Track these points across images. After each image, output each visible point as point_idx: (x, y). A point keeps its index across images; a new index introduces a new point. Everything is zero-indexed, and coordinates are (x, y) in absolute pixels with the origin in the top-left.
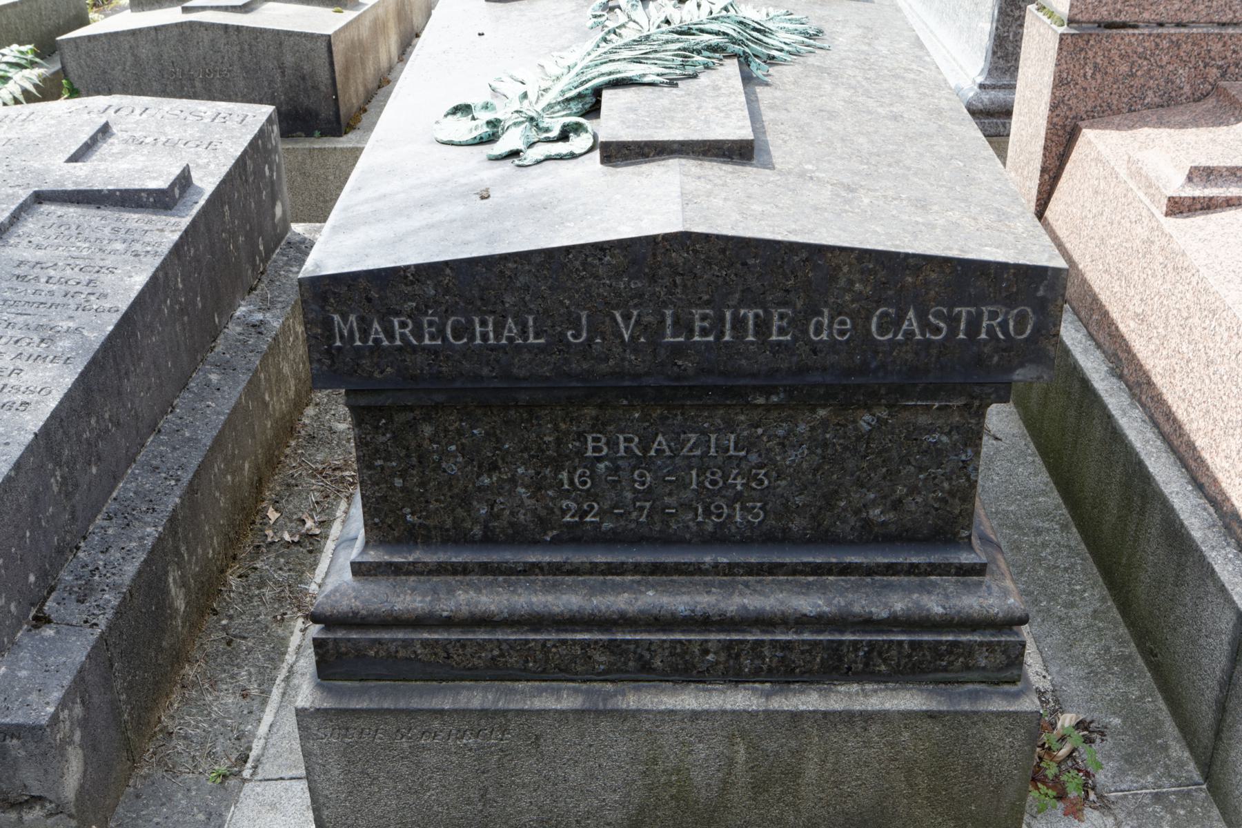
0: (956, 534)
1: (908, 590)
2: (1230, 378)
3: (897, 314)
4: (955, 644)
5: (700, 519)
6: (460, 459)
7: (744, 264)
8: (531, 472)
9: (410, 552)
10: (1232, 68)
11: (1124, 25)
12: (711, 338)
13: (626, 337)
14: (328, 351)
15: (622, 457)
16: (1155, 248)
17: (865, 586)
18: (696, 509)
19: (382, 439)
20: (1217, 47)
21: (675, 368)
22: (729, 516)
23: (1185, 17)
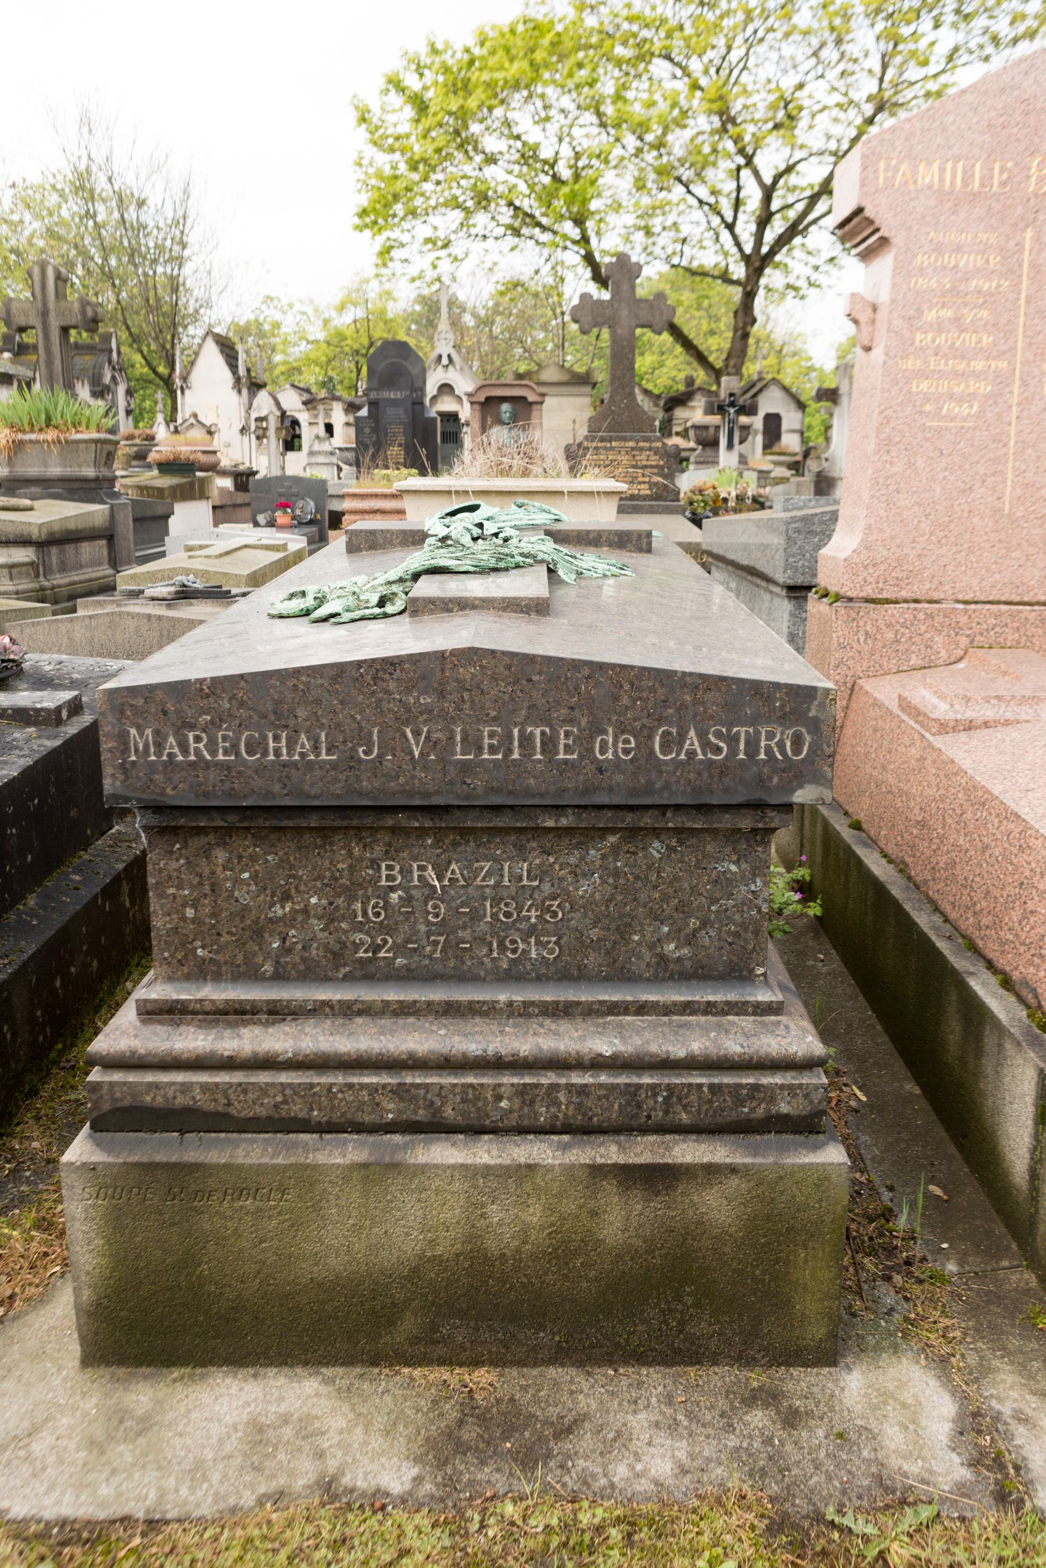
1: (705, 1030)
2: (1005, 857)
3: (678, 733)
4: (756, 1087)
5: (495, 955)
6: (253, 888)
7: (529, 680)
8: (324, 902)
10: (978, 637)
11: (888, 601)
12: (500, 756)
13: (417, 754)
14: (122, 766)
15: (415, 887)
16: (928, 762)
18: (491, 944)
19: (174, 865)
20: (963, 619)
21: (465, 787)
23: (936, 596)
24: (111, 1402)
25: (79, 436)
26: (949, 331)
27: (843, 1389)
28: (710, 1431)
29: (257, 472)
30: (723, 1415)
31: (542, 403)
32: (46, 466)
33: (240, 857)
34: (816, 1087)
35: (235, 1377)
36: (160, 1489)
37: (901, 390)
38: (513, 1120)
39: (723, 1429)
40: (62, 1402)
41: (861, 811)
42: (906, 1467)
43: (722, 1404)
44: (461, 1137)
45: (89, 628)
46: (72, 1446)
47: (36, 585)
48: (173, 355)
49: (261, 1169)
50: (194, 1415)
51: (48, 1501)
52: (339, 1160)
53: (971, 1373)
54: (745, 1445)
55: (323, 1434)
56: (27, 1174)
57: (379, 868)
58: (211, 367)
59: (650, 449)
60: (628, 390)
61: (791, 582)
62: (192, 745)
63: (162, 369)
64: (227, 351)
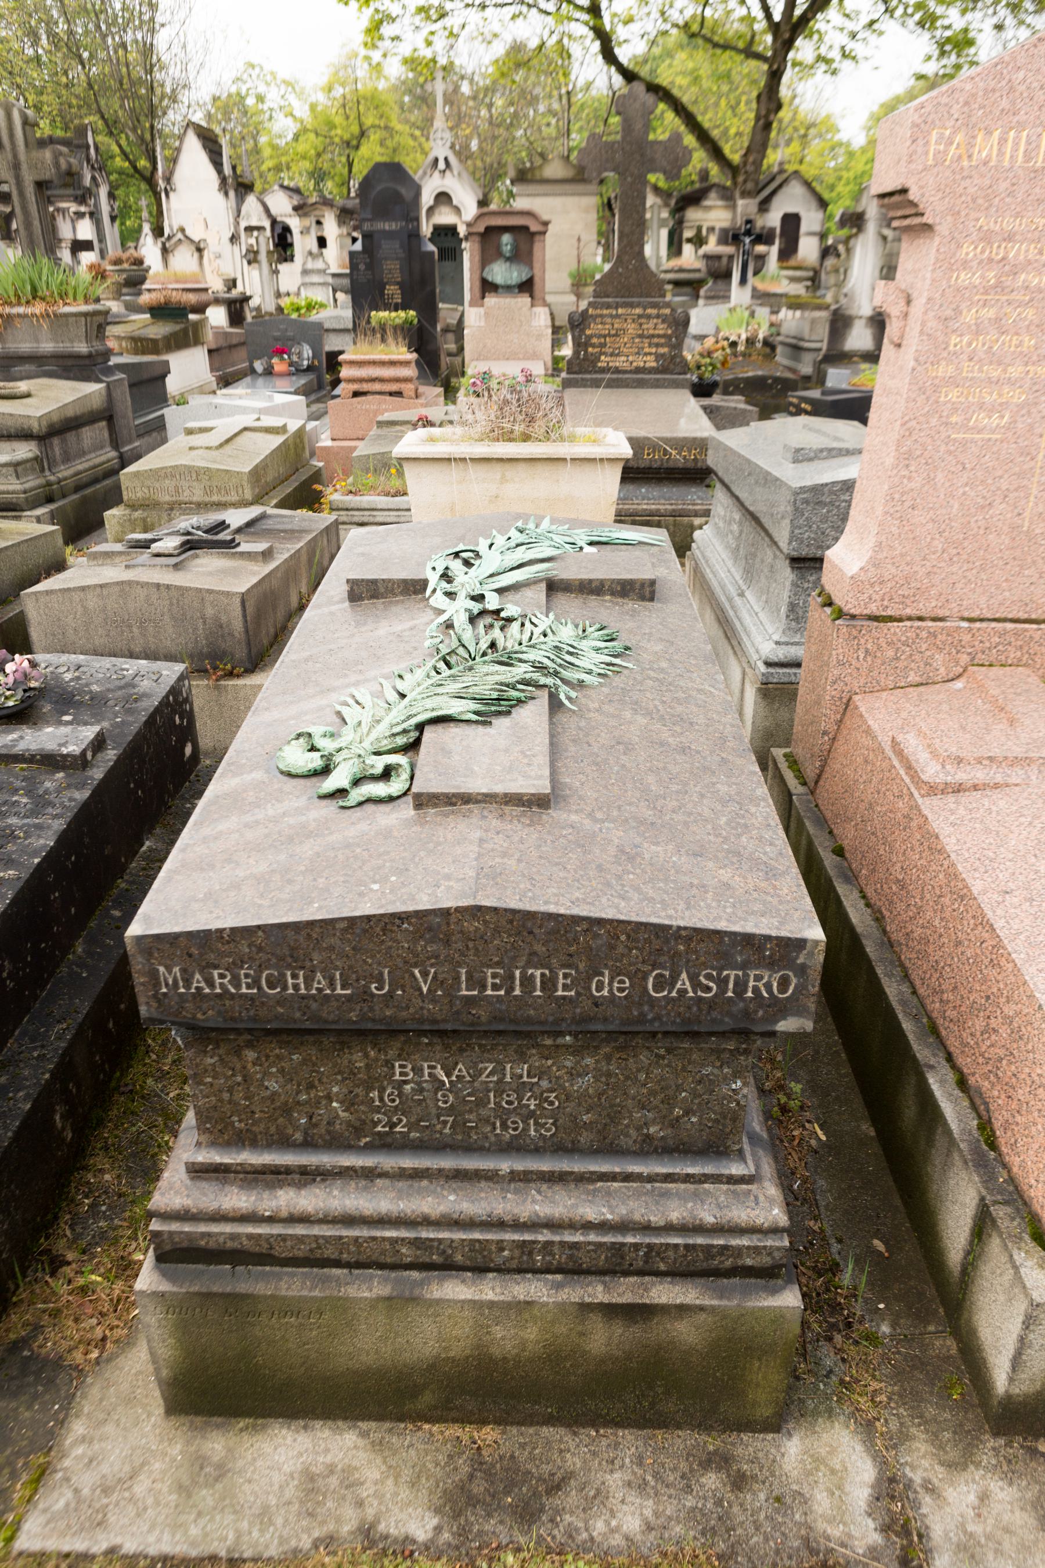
0: (727, 1148)
1: (683, 1198)
4: (725, 1247)
5: (498, 1131)
7: (531, 933)
9: (238, 1153)
12: (502, 993)
13: (425, 990)
14: (155, 996)
16: (914, 824)
17: (645, 1194)
18: (494, 1124)
20: (966, 638)
22: (524, 1129)
23: (941, 613)
24: (193, 1449)
25: (67, 309)
26: (988, 333)
27: (783, 1455)
28: (672, 1491)
29: (250, 297)
30: (683, 1476)
31: (544, 233)
32: (37, 341)
33: (267, 1057)
34: (778, 1249)
35: (289, 1428)
36: (237, 1531)
37: (928, 399)
38: (514, 1264)
39: (682, 1490)
40: (154, 1447)
41: (847, 835)
42: (829, 1531)
43: (683, 1466)
44: (469, 1274)
45: (100, 596)
46: (165, 1489)
47: (41, 481)
48: (154, 151)
49: (301, 1299)
50: (259, 1463)
51: (151, 1539)
52: (366, 1294)
53: (891, 1439)
54: (700, 1505)
55: (362, 1484)
56: (104, 1208)
57: (393, 1067)
58: (194, 170)
59: (658, 316)
60: (636, 249)
61: (795, 554)
62: (218, 981)
63: (143, 163)
64: (210, 145)
